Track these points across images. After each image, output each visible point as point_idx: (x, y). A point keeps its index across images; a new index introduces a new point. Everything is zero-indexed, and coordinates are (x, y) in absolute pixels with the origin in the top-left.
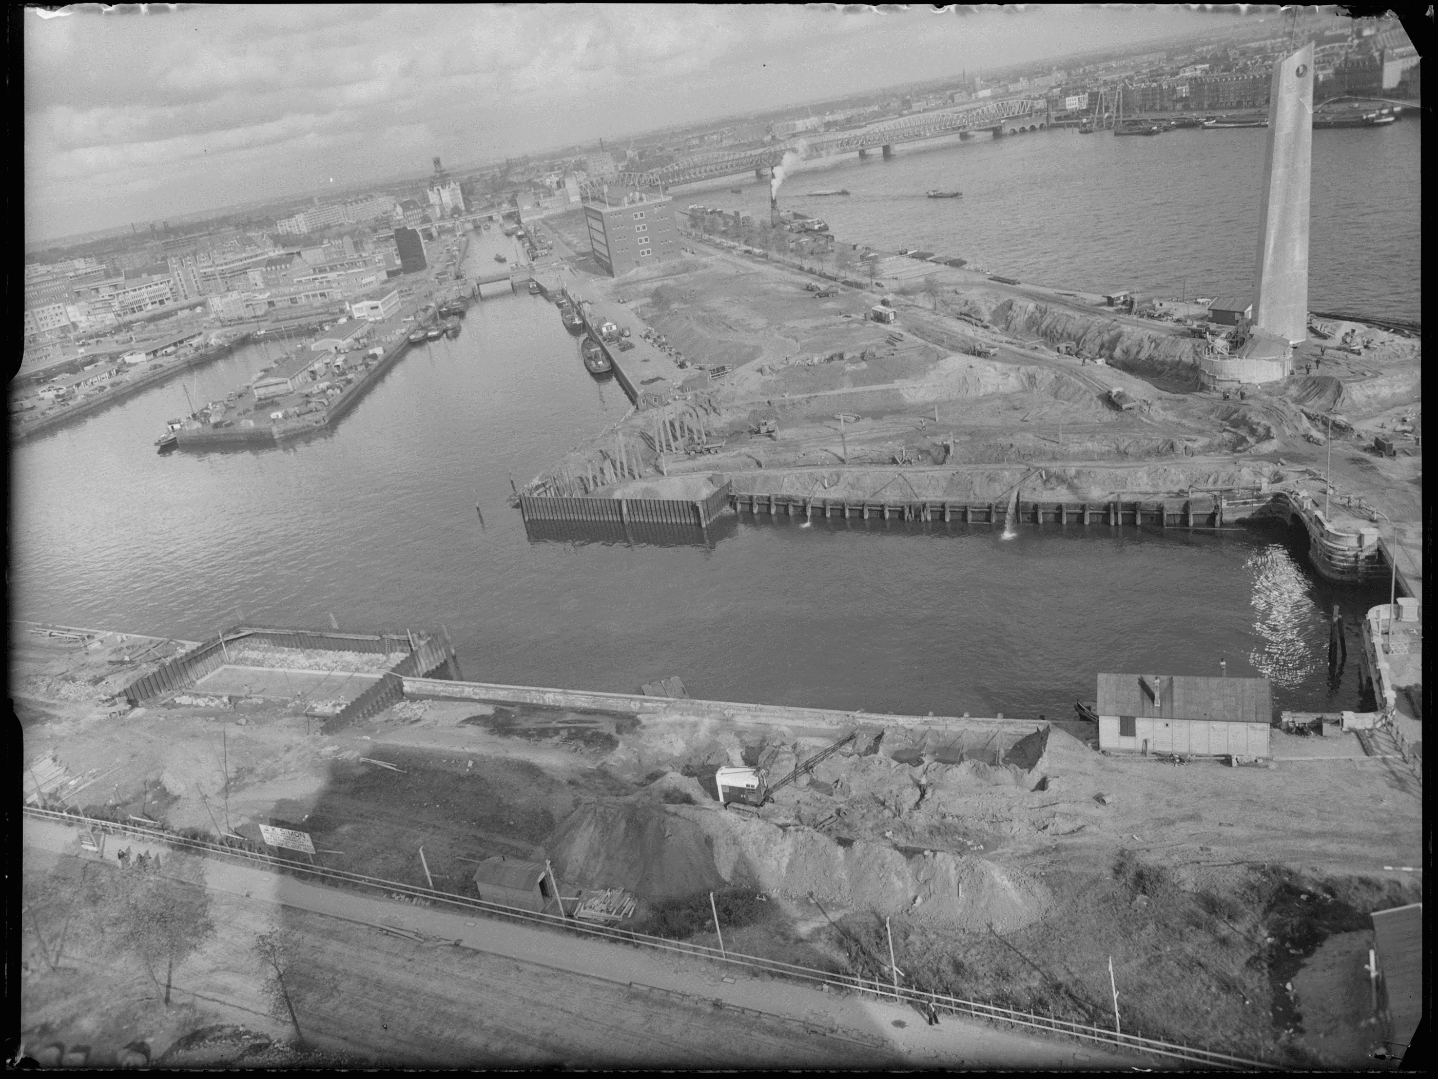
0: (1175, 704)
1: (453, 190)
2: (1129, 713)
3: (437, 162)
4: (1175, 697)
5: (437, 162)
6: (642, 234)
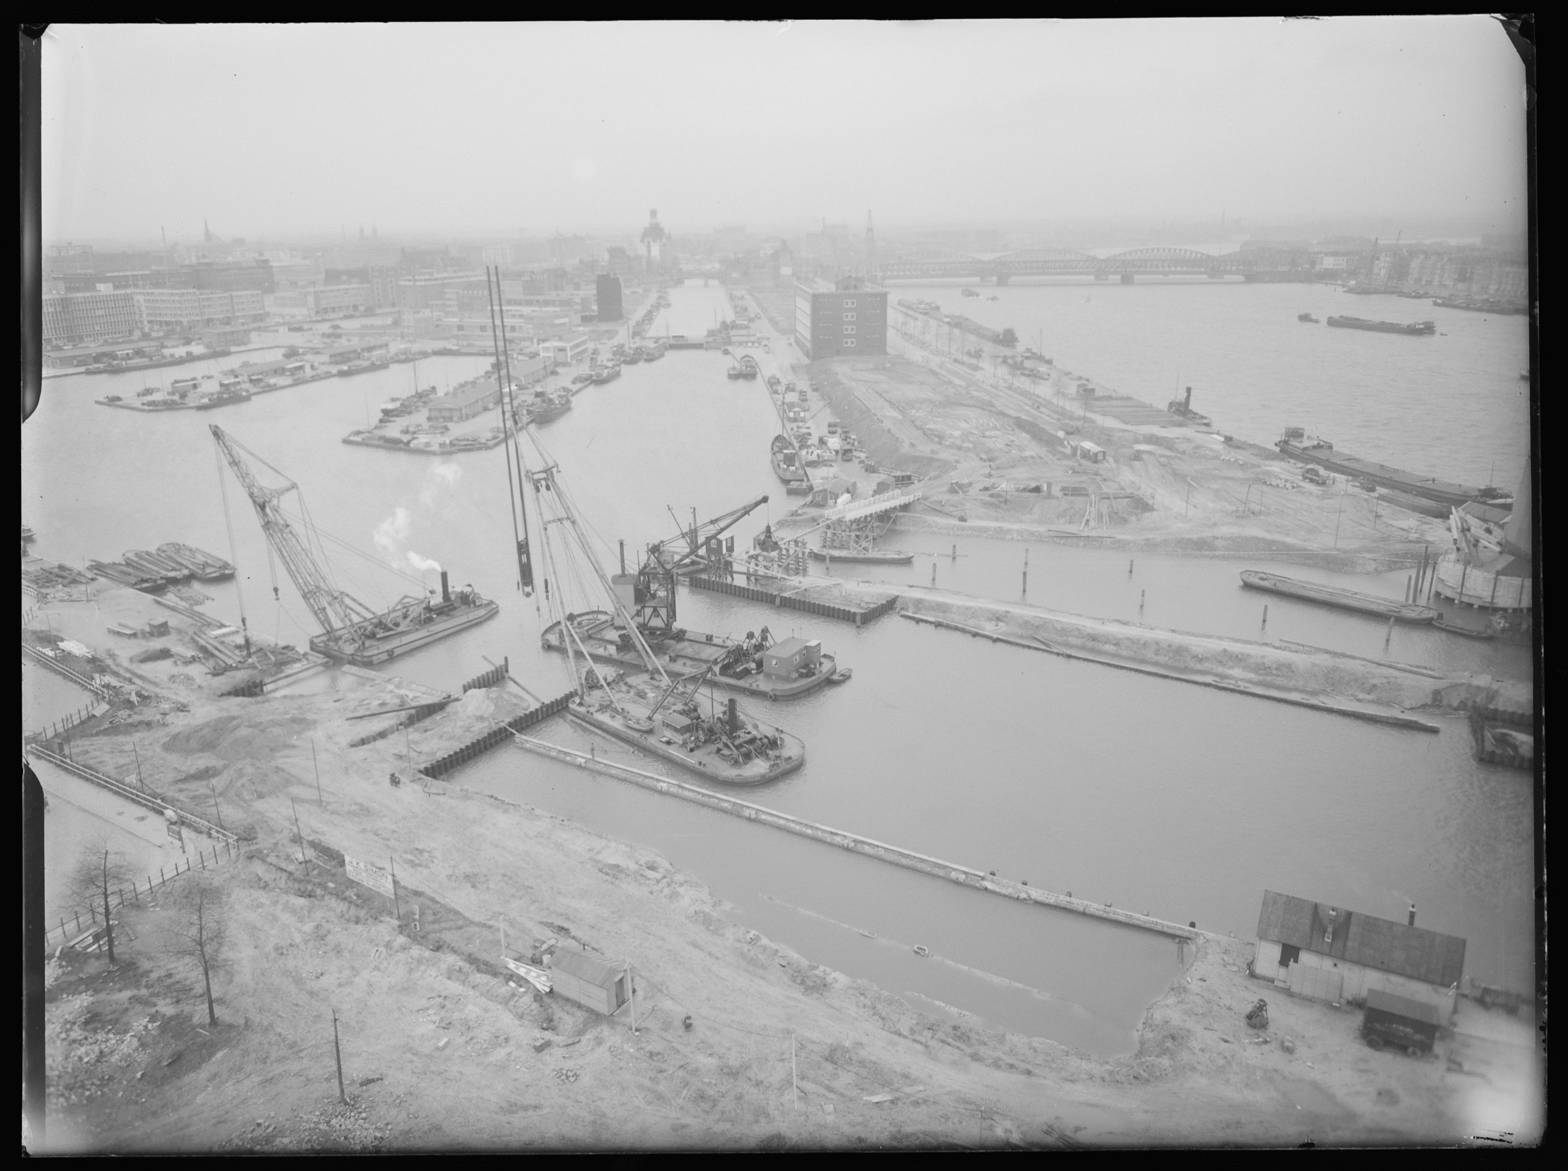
0: (1350, 944)
2: (1294, 941)
3: (654, 213)
4: (1351, 935)
5: (654, 213)
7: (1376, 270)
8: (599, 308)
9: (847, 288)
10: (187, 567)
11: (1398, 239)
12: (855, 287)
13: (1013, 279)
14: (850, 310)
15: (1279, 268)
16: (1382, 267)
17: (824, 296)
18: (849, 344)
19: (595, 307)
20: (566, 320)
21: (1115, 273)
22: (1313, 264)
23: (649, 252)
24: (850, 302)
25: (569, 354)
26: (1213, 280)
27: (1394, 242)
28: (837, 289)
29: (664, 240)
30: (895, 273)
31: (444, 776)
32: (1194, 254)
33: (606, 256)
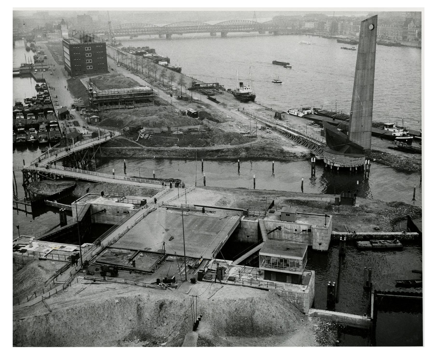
6: (89, 58)
7: (325, 28)
8: (327, 141)
9: (86, 41)
10: (335, 294)
11: (334, 15)
12: (90, 41)
13: (229, 34)
15: (288, 28)
16: (327, 26)
17: (76, 45)
21: (219, 32)
22: (301, 26)
24: (88, 48)
26: (261, 35)
27: (332, 16)
28: (81, 42)
30: (121, 34)
31: (275, 148)
32: (249, 22)
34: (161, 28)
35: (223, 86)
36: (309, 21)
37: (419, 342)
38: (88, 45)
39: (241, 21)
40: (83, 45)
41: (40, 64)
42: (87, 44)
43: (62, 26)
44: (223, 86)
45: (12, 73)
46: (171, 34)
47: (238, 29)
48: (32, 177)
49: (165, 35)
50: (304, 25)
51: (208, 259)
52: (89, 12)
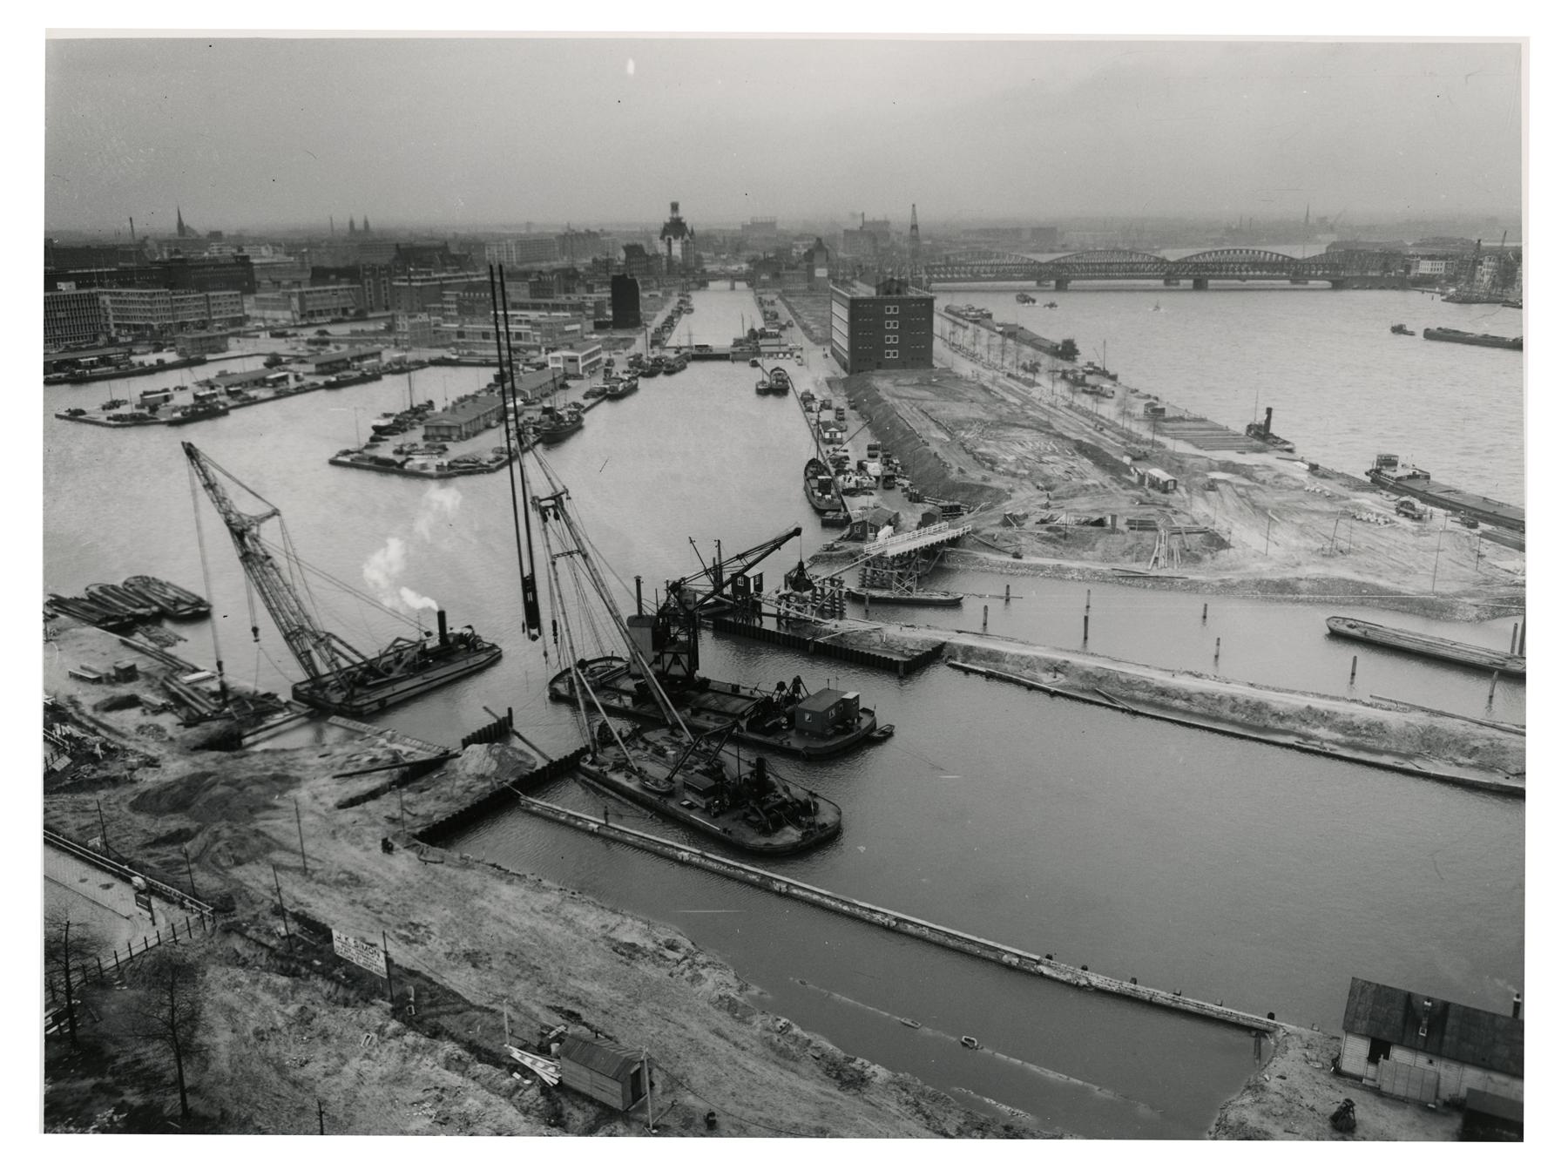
1: (687, 242)
5: (675, 207)
6: (892, 332)
7: (1478, 276)
9: (889, 293)
12: (898, 292)
14: (892, 317)
15: (1370, 274)
18: (891, 356)
19: (610, 313)
20: (577, 327)
23: (670, 250)
24: (892, 308)
25: (581, 365)
27: (1499, 244)
28: (878, 294)
29: (687, 237)
33: (622, 255)
34: (1046, 264)
35: (569, 498)
36: (1431, 257)
37: (1520, 1138)
38: (892, 302)
39: (1247, 251)
40: (882, 300)
41: (775, 341)
42: (892, 299)
43: (817, 254)
44: (569, 498)
45: (41, 377)
46: (1068, 281)
47: (1230, 273)
48: (226, 704)
49: (1053, 283)
50: (1417, 267)
51: (603, 1106)
52: (986, 232)
